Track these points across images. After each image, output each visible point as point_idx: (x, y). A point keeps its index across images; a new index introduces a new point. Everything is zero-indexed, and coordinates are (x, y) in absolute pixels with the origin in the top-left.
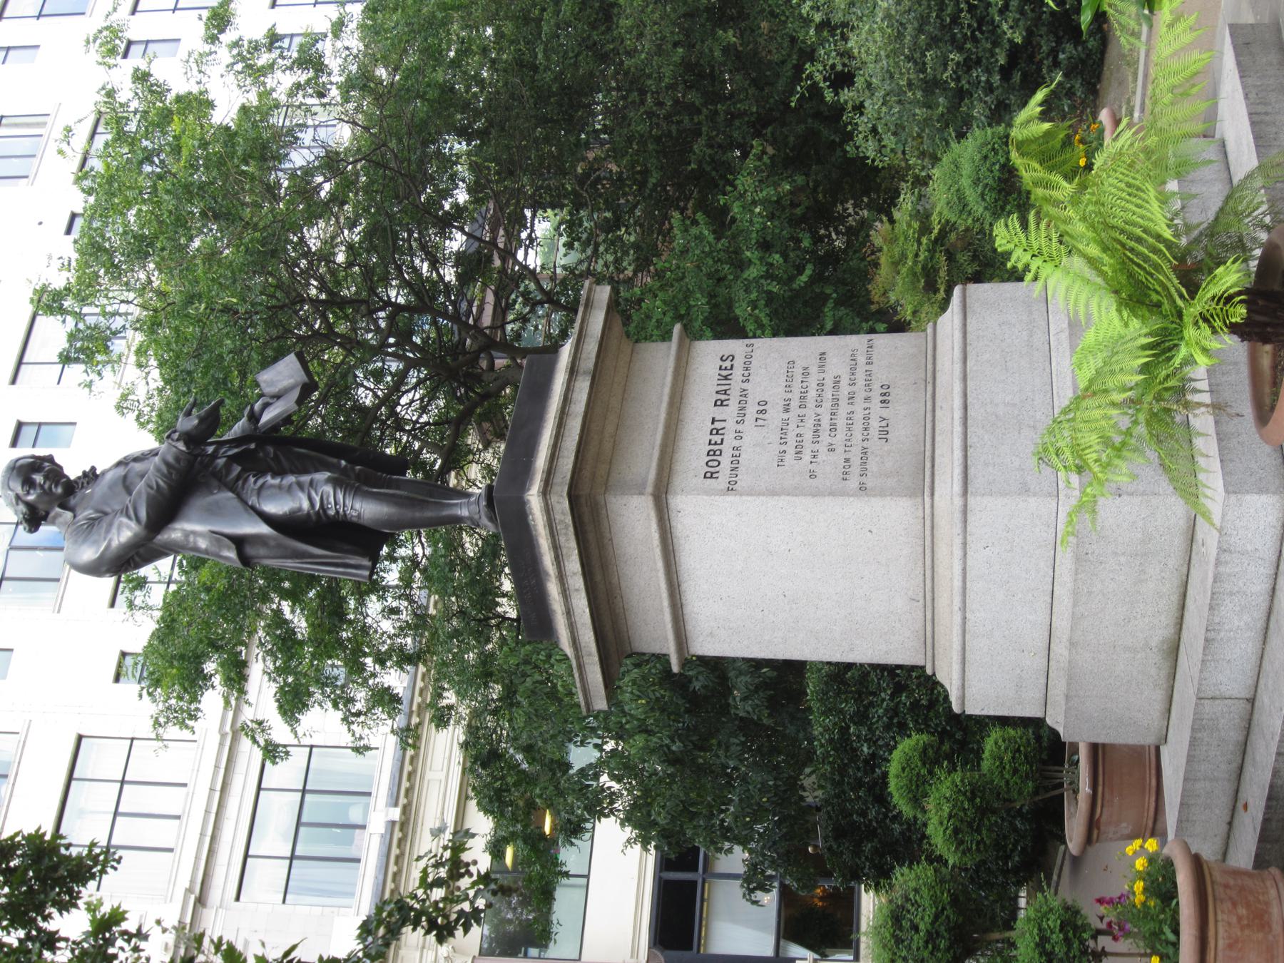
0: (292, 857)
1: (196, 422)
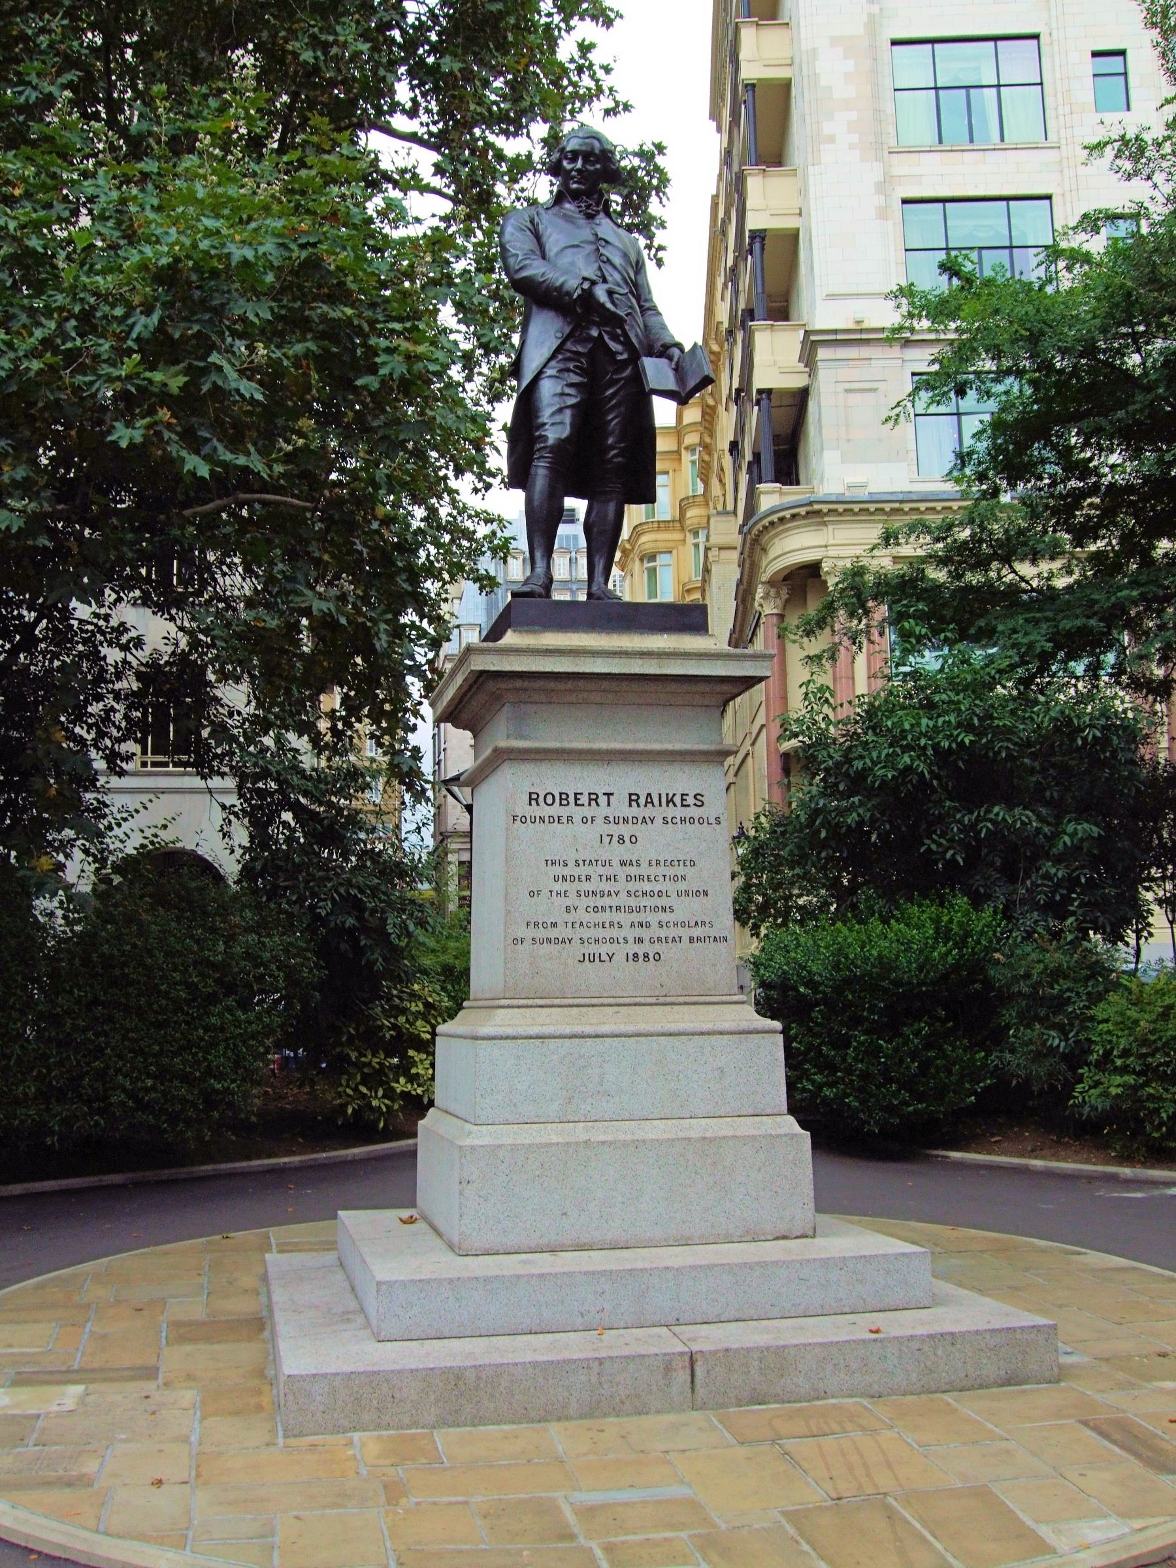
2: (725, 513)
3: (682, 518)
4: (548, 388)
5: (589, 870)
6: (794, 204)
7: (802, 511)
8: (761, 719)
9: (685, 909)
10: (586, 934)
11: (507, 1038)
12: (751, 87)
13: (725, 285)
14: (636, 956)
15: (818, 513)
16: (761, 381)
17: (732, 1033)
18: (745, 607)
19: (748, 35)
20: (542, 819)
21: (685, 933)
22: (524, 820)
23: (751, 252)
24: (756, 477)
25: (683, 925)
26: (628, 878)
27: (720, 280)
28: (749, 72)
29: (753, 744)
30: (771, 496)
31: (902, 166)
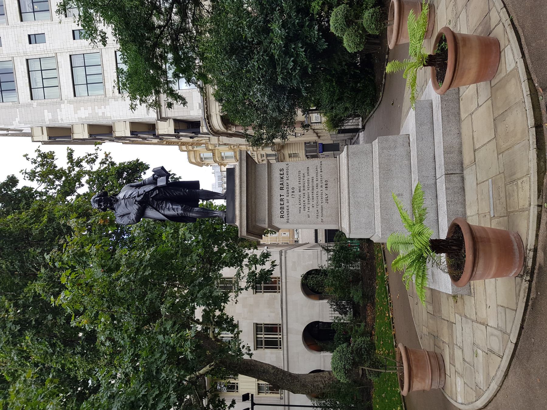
2: (209, 139)
4: (167, 212)
5: (302, 201)
6: (122, 123)
9: (312, 174)
12: (90, 135)
14: (326, 187)
16: (173, 132)
19: (76, 136)
21: (319, 173)
24: (199, 133)
27: (146, 141)
28: (86, 136)
30: (204, 129)
31: (109, 93)
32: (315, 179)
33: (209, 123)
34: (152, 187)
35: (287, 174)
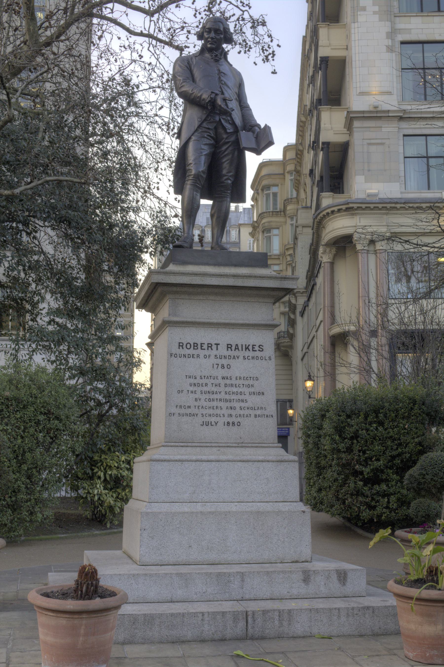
0: (427, 157)
1: (220, 104)
2: (306, 208)
3: (284, 211)
7: (344, 207)
8: (321, 318)
10: (204, 412)
11: (165, 461)
13: (309, 85)
14: (228, 423)
15: (352, 208)
16: (323, 138)
17: (273, 461)
18: (314, 258)
20: (185, 356)
21: (252, 413)
22: (176, 356)
23: (320, 68)
24: (321, 190)
25: (252, 408)
26: (226, 385)
27: (307, 82)
29: (317, 331)
30: (328, 200)
32: (243, 405)
33: (339, 210)
34: (238, 121)
35: (253, 358)
